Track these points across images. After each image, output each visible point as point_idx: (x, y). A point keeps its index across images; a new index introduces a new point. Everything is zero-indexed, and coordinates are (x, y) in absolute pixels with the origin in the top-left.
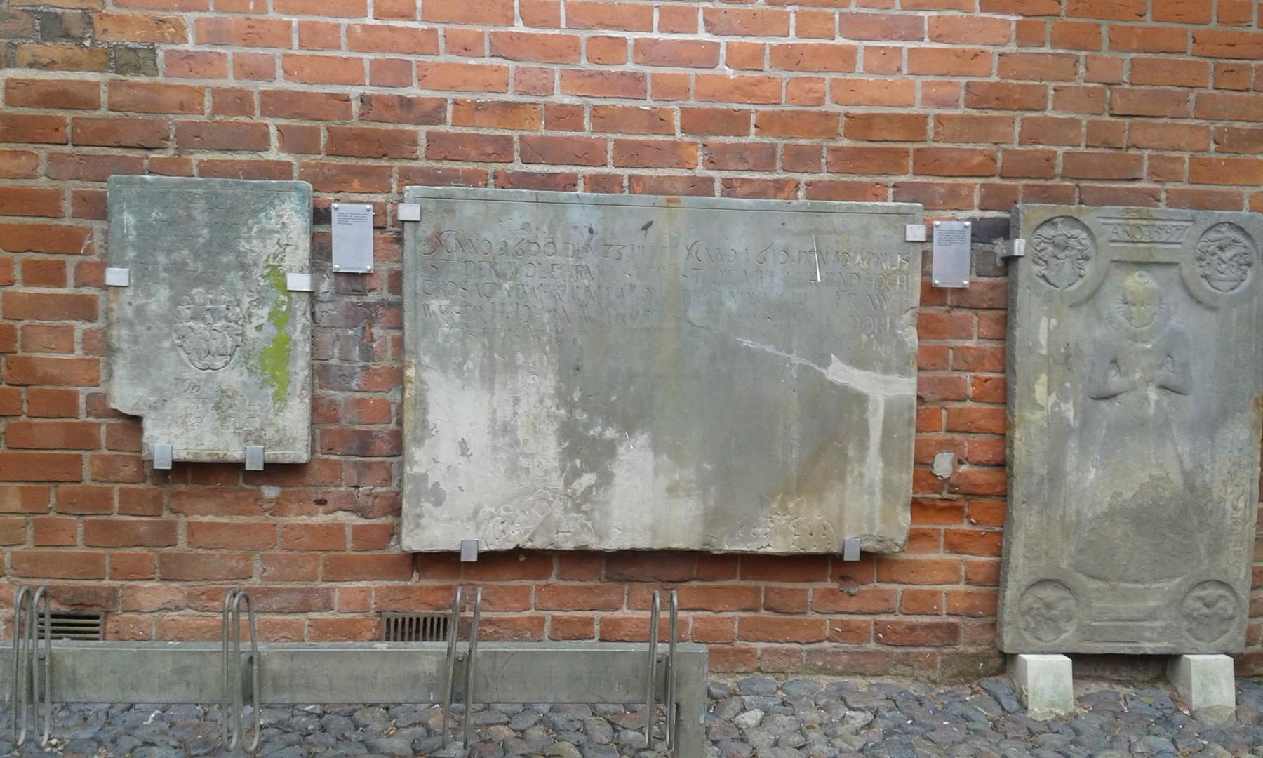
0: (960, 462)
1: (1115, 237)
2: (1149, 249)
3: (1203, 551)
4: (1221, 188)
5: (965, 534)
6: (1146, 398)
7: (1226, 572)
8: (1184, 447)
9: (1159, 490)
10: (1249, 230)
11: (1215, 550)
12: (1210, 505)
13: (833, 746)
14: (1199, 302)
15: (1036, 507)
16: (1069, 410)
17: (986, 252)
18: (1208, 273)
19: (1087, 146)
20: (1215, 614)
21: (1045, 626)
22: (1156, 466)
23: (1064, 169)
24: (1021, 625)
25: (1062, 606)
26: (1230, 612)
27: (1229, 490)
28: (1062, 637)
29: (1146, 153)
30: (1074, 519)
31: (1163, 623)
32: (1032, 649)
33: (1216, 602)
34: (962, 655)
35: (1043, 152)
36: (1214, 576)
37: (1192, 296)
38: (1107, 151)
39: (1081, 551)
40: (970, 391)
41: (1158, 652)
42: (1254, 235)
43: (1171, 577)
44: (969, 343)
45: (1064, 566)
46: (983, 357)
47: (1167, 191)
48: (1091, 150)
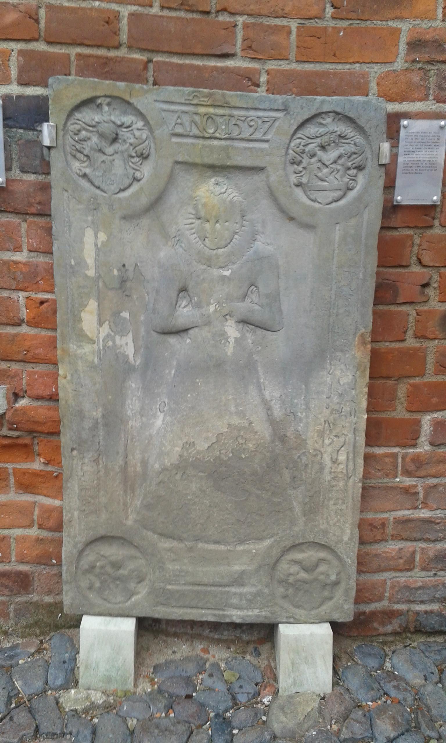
0: (16, 396)
1: (179, 130)
2: (226, 149)
3: (298, 510)
4: (340, 67)
5: (36, 474)
6: (223, 335)
7: (325, 532)
8: (272, 392)
9: (240, 441)
10: (361, 122)
11: (312, 509)
12: (304, 459)
13: (321, 434)
14: (291, 219)
15: (89, 456)
16: (127, 345)
17: (28, 141)
18: (304, 180)
19: (162, 8)
20: (316, 580)
21: (112, 586)
22: (239, 414)
23: (130, 36)
24: (84, 583)
25: (131, 565)
26: (333, 578)
27: (327, 442)
28: (133, 599)
29: (240, 20)
30: (139, 469)
31: (253, 590)
32: (97, 610)
33: (317, 566)
34: (37, 605)
35: (99, 10)
36: (310, 538)
37: (282, 210)
38: (190, 16)
39: (148, 507)
40: (24, 313)
41: (249, 621)
42: (367, 128)
43: (260, 539)
44: (18, 257)
45: (130, 522)
46: (36, 274)
47: (268, 72)
48: (166, 13)
